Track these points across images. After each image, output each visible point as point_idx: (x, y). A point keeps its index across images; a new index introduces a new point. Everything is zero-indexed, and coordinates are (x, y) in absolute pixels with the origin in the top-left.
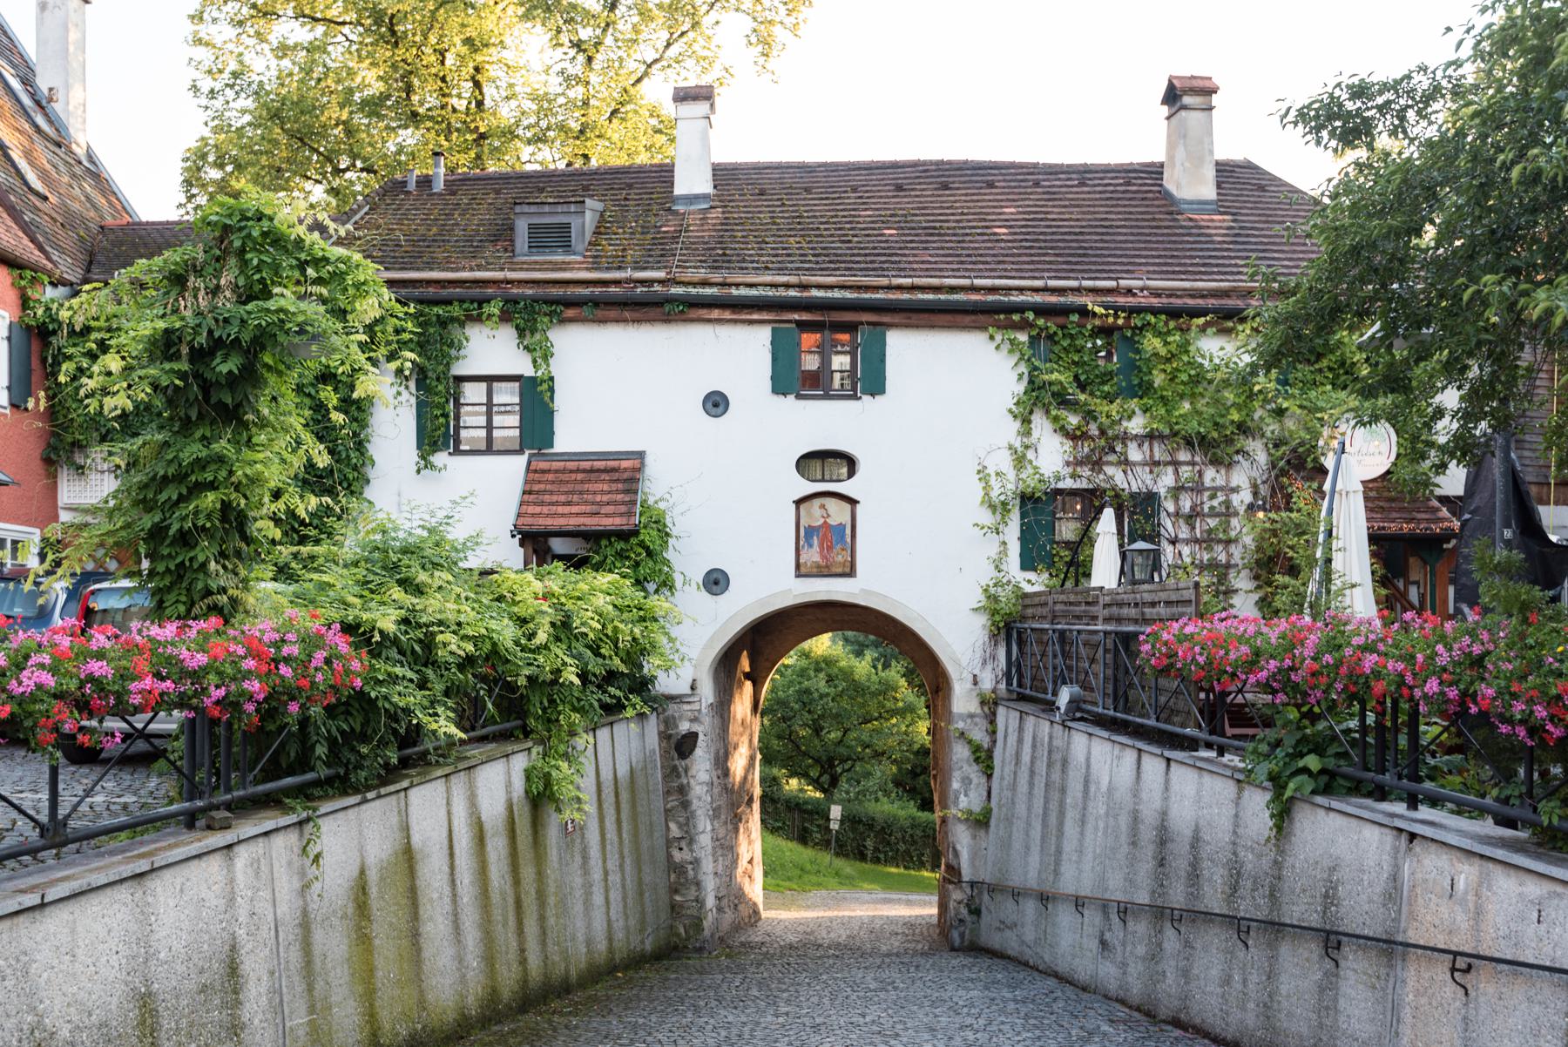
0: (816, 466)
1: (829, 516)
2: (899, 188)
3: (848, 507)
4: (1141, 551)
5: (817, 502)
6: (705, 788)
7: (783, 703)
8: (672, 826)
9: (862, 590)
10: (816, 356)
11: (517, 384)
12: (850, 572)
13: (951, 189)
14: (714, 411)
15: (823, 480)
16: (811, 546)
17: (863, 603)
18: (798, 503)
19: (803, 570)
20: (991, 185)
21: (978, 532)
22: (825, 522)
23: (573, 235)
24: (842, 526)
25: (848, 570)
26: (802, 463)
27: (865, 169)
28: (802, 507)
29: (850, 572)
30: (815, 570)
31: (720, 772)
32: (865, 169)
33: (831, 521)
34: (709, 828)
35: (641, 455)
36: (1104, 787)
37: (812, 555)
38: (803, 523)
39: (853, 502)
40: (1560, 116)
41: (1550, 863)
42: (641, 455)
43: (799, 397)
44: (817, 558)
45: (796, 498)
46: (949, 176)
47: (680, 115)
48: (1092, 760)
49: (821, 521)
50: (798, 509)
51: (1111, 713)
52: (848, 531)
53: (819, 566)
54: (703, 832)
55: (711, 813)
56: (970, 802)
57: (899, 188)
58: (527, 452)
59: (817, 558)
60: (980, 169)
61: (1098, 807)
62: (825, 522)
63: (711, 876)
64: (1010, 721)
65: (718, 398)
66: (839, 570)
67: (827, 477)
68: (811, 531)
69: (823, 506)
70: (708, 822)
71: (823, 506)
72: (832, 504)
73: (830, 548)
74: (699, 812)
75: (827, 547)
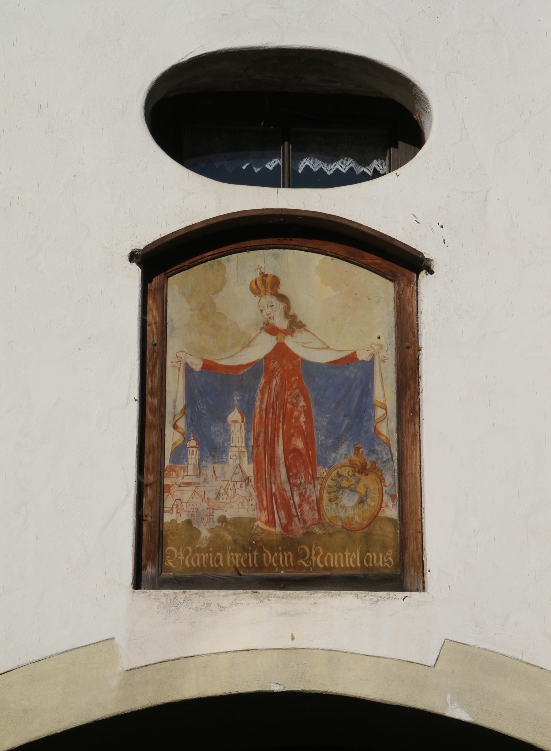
41: (276, 511)
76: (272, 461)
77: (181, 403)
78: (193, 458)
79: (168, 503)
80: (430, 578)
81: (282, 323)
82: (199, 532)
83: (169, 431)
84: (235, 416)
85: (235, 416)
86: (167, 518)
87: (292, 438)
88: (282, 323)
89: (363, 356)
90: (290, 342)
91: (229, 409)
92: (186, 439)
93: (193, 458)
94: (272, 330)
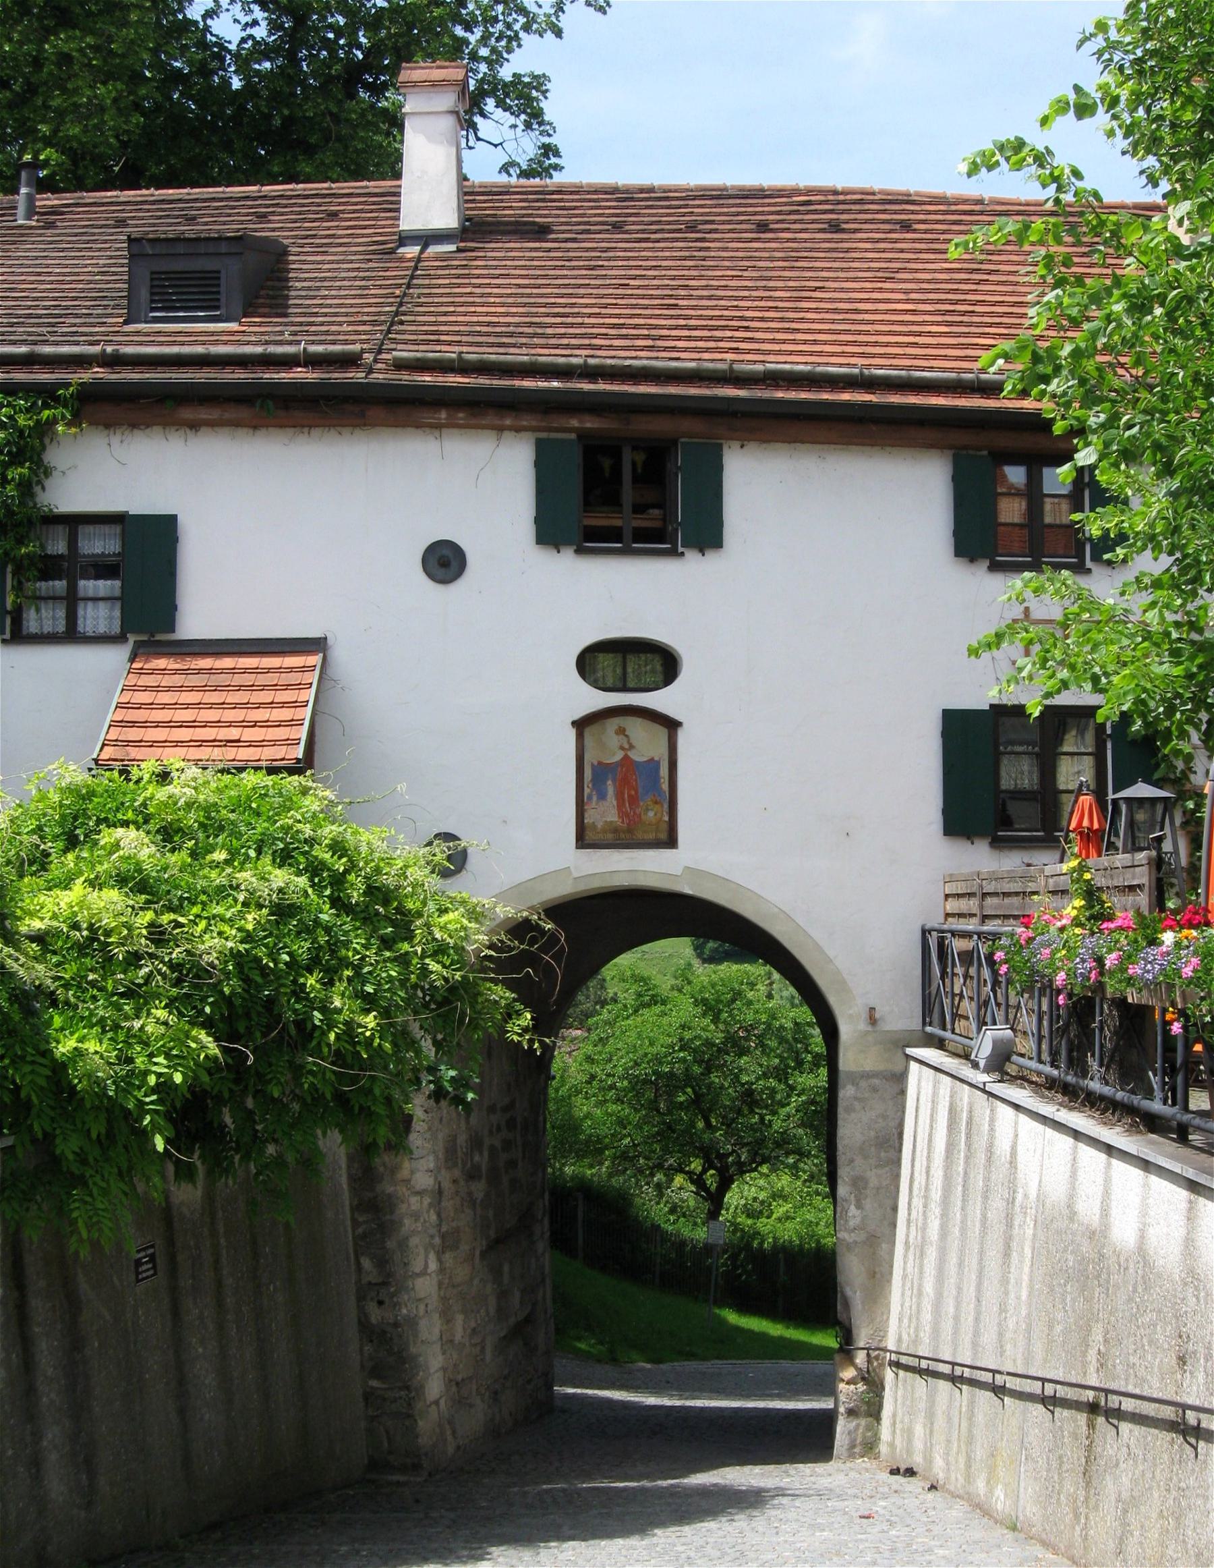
0: (606, 661)
1: (631, 747)
2: (763, 227)
3: (662, 733)
4: (1141, 801)
5: (613, 723)
6: (427, 1201)
7: (9, 999)
8: (366, 1263)
9: (687, 868)
10: (1062, 787)
11: (117, 529)
12: (671, 842)
13: (843, 231)
14: (440, 572)
15: (624, 689)
16: (602, 796)
17: (688, 891)
18: (581, 725)
19: (590, 836)
20: (906, 226)
22: (626, 758)
23: (223, 289)
24: (653, 764)
25: (663, 836)
27: (713, 197)
29: (671, 842)
30: (610, 836)
31: (457, 1173)
32: (713, 197)
33: (636, 756)
34: (433, 1266)
36: (1033, 1194)
37: (605, 813)
38: (589, 758)
39: (671, 725)
43: (580, 551)
44: (613, 816)
46: (843, 212)
48: (1019, 1148)
49: (618, 756)
50: (580, 737)
51: (1047, 1069)
52: (664, 771)
53: (616, 831)
54: (424, 1273)
55: (437, 1241)
56: (864, 1218)
57: (763, 227)
58: (132, 639)
59: (613, 816)
60: (891, 202)
61: (1026, 1229)
62: (626, 758)
63: (437, 1348)
64: (923, 1084)
65: (446, 552)
66: (651, 836)
67: (631, 684)
68: (602, 771)
69: (621, 731)
70: (432, 1257)
71: (621, 731)
72: (638, 729)
73: (634, 801)
74: (414, 1241)
75: (628, 800)
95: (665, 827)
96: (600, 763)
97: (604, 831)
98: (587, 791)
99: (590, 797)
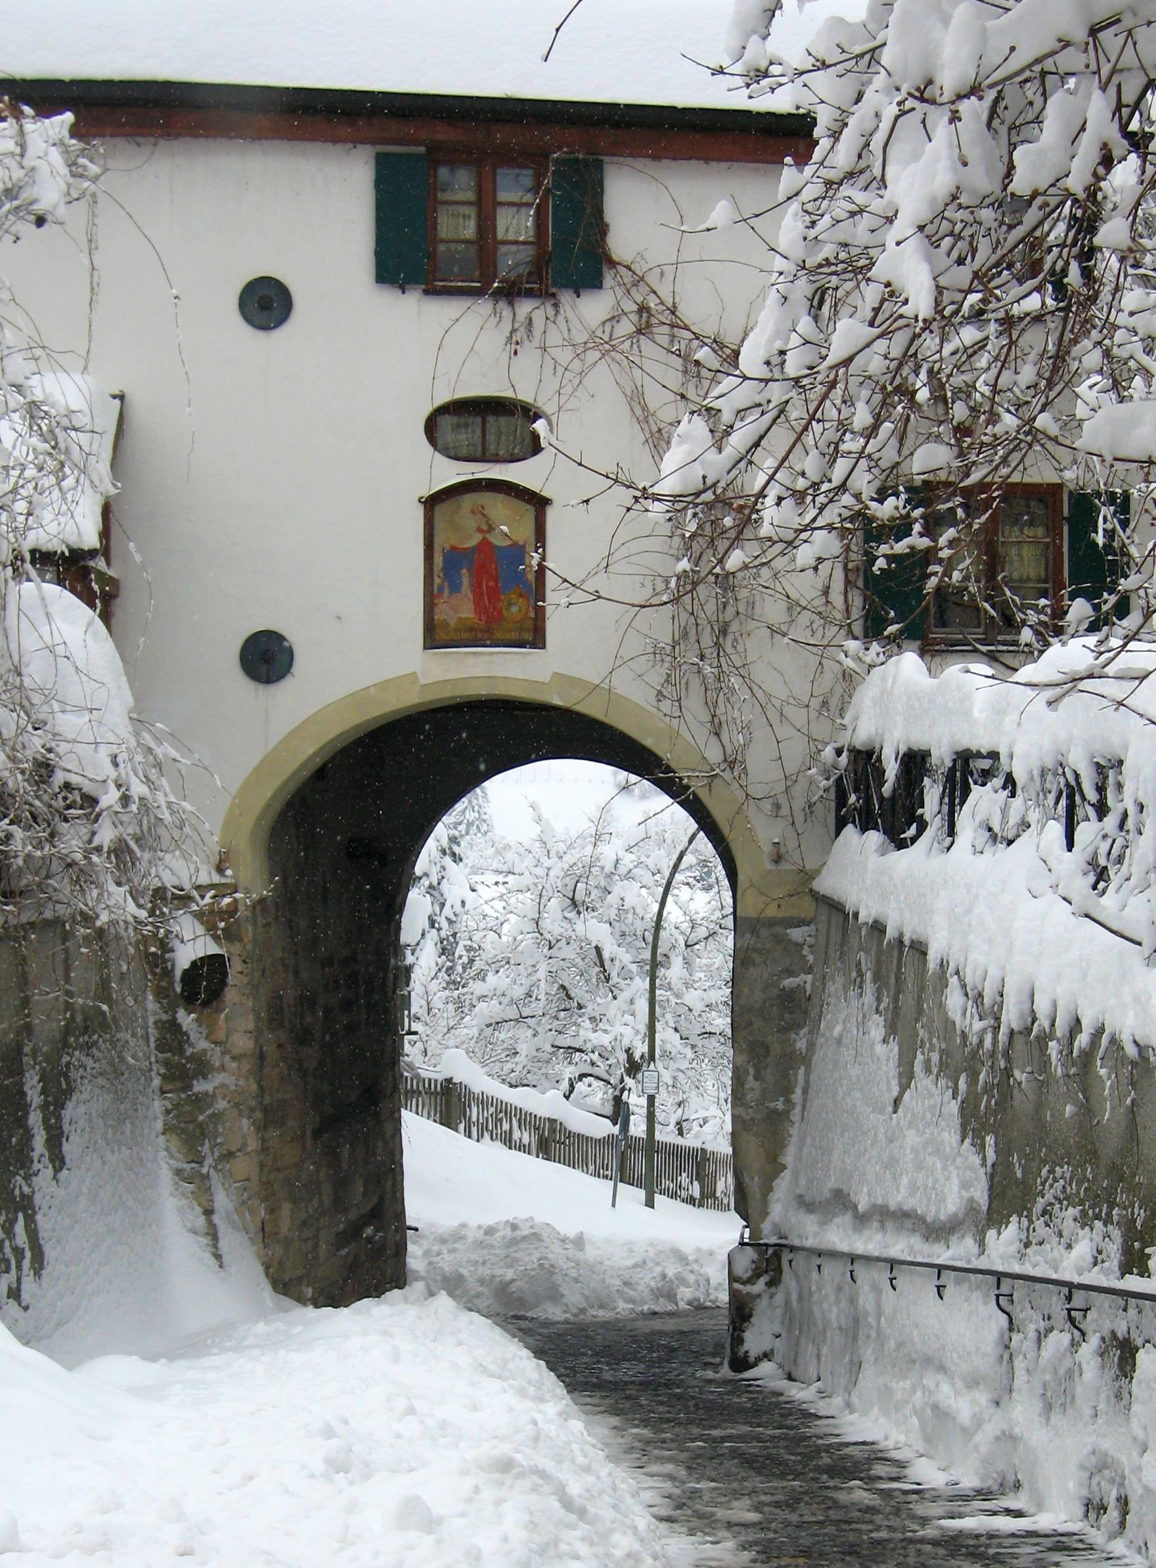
3: (529, 512)
9: (556, 675)
16: (455, 588)
18: (432, 503)
19: (441, 635)
21: (895, 744)
26: (446, 421)
28: (440, 510)
35: (544, 647)
38: (439, 541)
39: (539, 503)
40: (906, 554)
41: (487, 466)
42: (544, 647)
45: (426, 493)
47: (686, 255)
49: (476, 539)
66: (514, 636)
68: (455, 557)
71: (479, 511)
72: (498, 507)
73: (494, 593)
76: (482, 594)
77: (441, 565)
78: (446, 591)
79: (436, 610)
80: (548, 644)
81: (485, 527)
82: (904, 1378)
83: (436, 578)
84: (464, 571)
85: (464, 571)
86: (436, 617)
87: (528, 168)
88: (485, 527)
89: (521, 543)
90: (488, 536)
91: (461, 569)
92: (443, 581)
93: (446, 591)
94: (479, 530)
95: (529, 624)
96: (453, 548)
97: (457, 630)
98: (437, 581)
99: (441, 589)
